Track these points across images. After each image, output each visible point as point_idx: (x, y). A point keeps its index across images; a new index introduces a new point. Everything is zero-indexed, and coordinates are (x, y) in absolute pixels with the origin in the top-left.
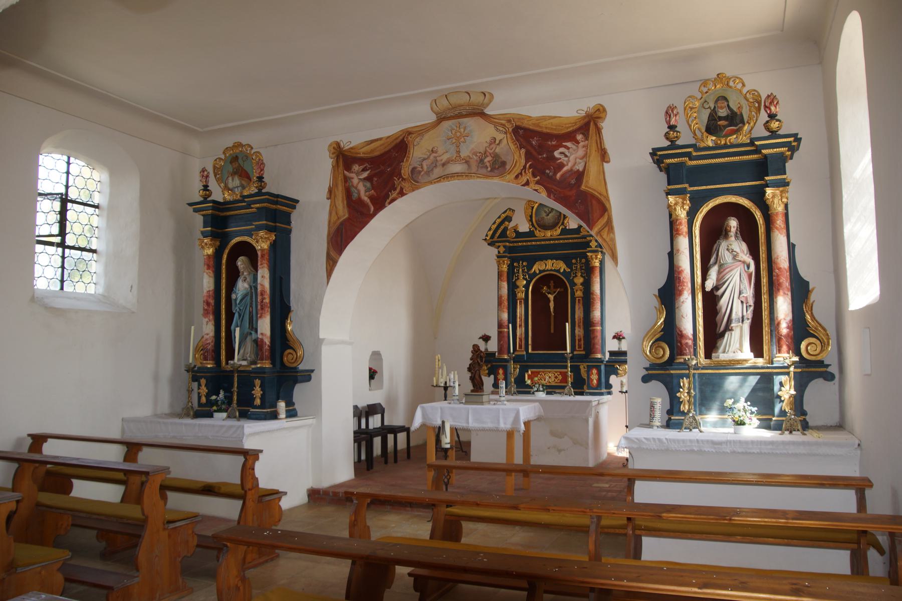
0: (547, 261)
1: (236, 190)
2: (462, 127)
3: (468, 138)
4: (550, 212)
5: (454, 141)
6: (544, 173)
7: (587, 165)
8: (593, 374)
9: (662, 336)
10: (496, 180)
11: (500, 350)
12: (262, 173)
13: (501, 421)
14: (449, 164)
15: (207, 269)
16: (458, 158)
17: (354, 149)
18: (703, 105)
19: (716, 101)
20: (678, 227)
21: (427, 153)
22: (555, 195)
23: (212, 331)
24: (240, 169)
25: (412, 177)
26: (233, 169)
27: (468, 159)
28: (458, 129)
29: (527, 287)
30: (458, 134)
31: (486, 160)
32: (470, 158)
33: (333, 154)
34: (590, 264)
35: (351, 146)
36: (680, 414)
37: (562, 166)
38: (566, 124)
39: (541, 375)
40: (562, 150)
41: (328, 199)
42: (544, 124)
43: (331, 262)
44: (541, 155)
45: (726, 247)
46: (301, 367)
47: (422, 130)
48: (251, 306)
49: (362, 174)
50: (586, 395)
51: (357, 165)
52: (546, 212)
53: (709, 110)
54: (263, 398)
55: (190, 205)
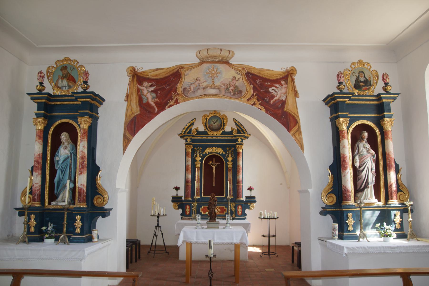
0: (213, 148)
1: (64, 88)
3: (219, 75)
4: (216, 122)
5: (211, 75)
6: (264, 99)
7: (287, 98)
8: (239, 209)
10: (236, 101)
11: (186, 196)
12: (87, 79)
13: (234, 239)
15: (39, 139)
16: (213, 85)
17: (145, 72)
19: (359, 73)
21: (194, 80)
22: (270, 112)
23: (40, 182)
24: (69, 75)
25: (184, 93)
26: (63, 75)
27: (219, 87)
28: (213, 69)
29: (201, 161)
30: (213, 72)
31: (230, 89)
32: (220, 86)
33: (130, 74)
34: (237, 151)
35: (143, 70)
36: (348, 232)
37: (273, 97)
40: (273, 88)
41: (125, 101)
42: (263, 73)
43: (127, 141)
44: (262, 89)
45: (363, 146)
46: (106, 207)
47: (191, 67)
48: (71, 164)
49: (150, 88)
50: (236, 220)
52: (213, 122)
53: (356, 77)
54: (82, 228)
55: (29, 94)
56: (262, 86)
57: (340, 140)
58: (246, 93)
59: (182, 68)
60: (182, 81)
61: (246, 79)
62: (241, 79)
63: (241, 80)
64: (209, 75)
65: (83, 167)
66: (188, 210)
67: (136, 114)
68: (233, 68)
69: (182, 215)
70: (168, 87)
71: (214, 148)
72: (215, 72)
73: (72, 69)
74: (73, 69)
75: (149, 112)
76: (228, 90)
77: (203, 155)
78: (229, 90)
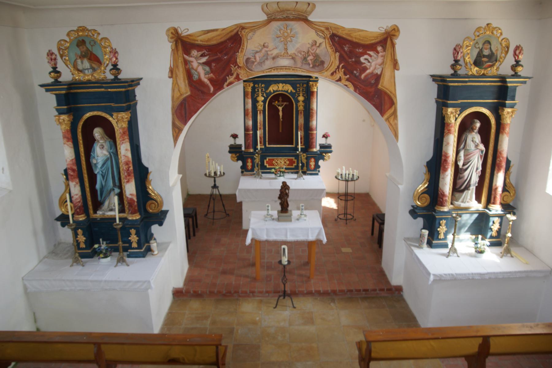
0: (279, 84)
1: (86, 72)
2: (289, 28)
3: (293, 38)
5: (282, 39)
9: (427, 191)
13: (310, 235)
14: (278, 58)
16: (286, 55)
18: (475, 45)
19: (484, 44)
20: (450, 128)
21: (260, 47)
24: (89, 53)
26: (81, 52)
27: (294, 56)
28: (285, 30)
29: (264, 102)
30: (286, 34)
32: (296, 55)
33: (172, 38)
35: (189, 33)
37: (365, 69)
38: (370, 37)
39: (275, 161)
40: (366, 56)
41: (170, 77)
42: (354, 35)
43: (177, 131)
44: (351, 59)
45: (471, 139)
47: (255, 27)
49: (201, 59)
51: (195, 51)
54: (139, 242)
55: (42, 86)
56: (351, 53)
57: (445, 134)
58: (329, 64)
59: (243, 28)
60: (243, 48)
61: (330, 44)
62: (324, 44)
63: (323, 45)
64: (281, 39)
65: (129, 175)
66: (249, 164)
67: (185, 96)
68: (313, 28)
69: (242, 168)
70: (225, 58)
71: (281, 84)
72: (288, 34)
73: (92, 43)
74: (94, 44)
75: (203, 92)
76: (305, 60)
77: (266, 94)
78: (307, 61)
